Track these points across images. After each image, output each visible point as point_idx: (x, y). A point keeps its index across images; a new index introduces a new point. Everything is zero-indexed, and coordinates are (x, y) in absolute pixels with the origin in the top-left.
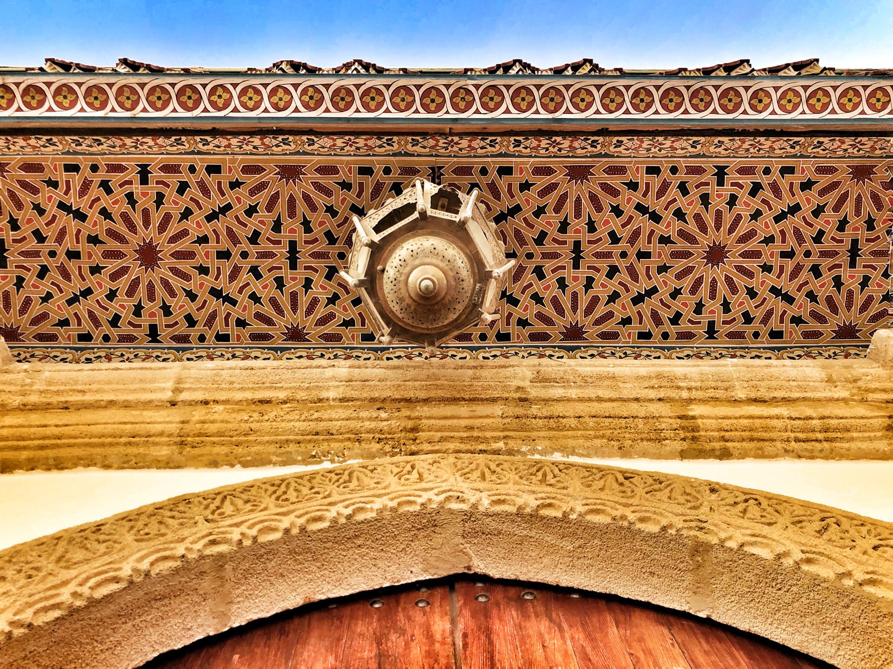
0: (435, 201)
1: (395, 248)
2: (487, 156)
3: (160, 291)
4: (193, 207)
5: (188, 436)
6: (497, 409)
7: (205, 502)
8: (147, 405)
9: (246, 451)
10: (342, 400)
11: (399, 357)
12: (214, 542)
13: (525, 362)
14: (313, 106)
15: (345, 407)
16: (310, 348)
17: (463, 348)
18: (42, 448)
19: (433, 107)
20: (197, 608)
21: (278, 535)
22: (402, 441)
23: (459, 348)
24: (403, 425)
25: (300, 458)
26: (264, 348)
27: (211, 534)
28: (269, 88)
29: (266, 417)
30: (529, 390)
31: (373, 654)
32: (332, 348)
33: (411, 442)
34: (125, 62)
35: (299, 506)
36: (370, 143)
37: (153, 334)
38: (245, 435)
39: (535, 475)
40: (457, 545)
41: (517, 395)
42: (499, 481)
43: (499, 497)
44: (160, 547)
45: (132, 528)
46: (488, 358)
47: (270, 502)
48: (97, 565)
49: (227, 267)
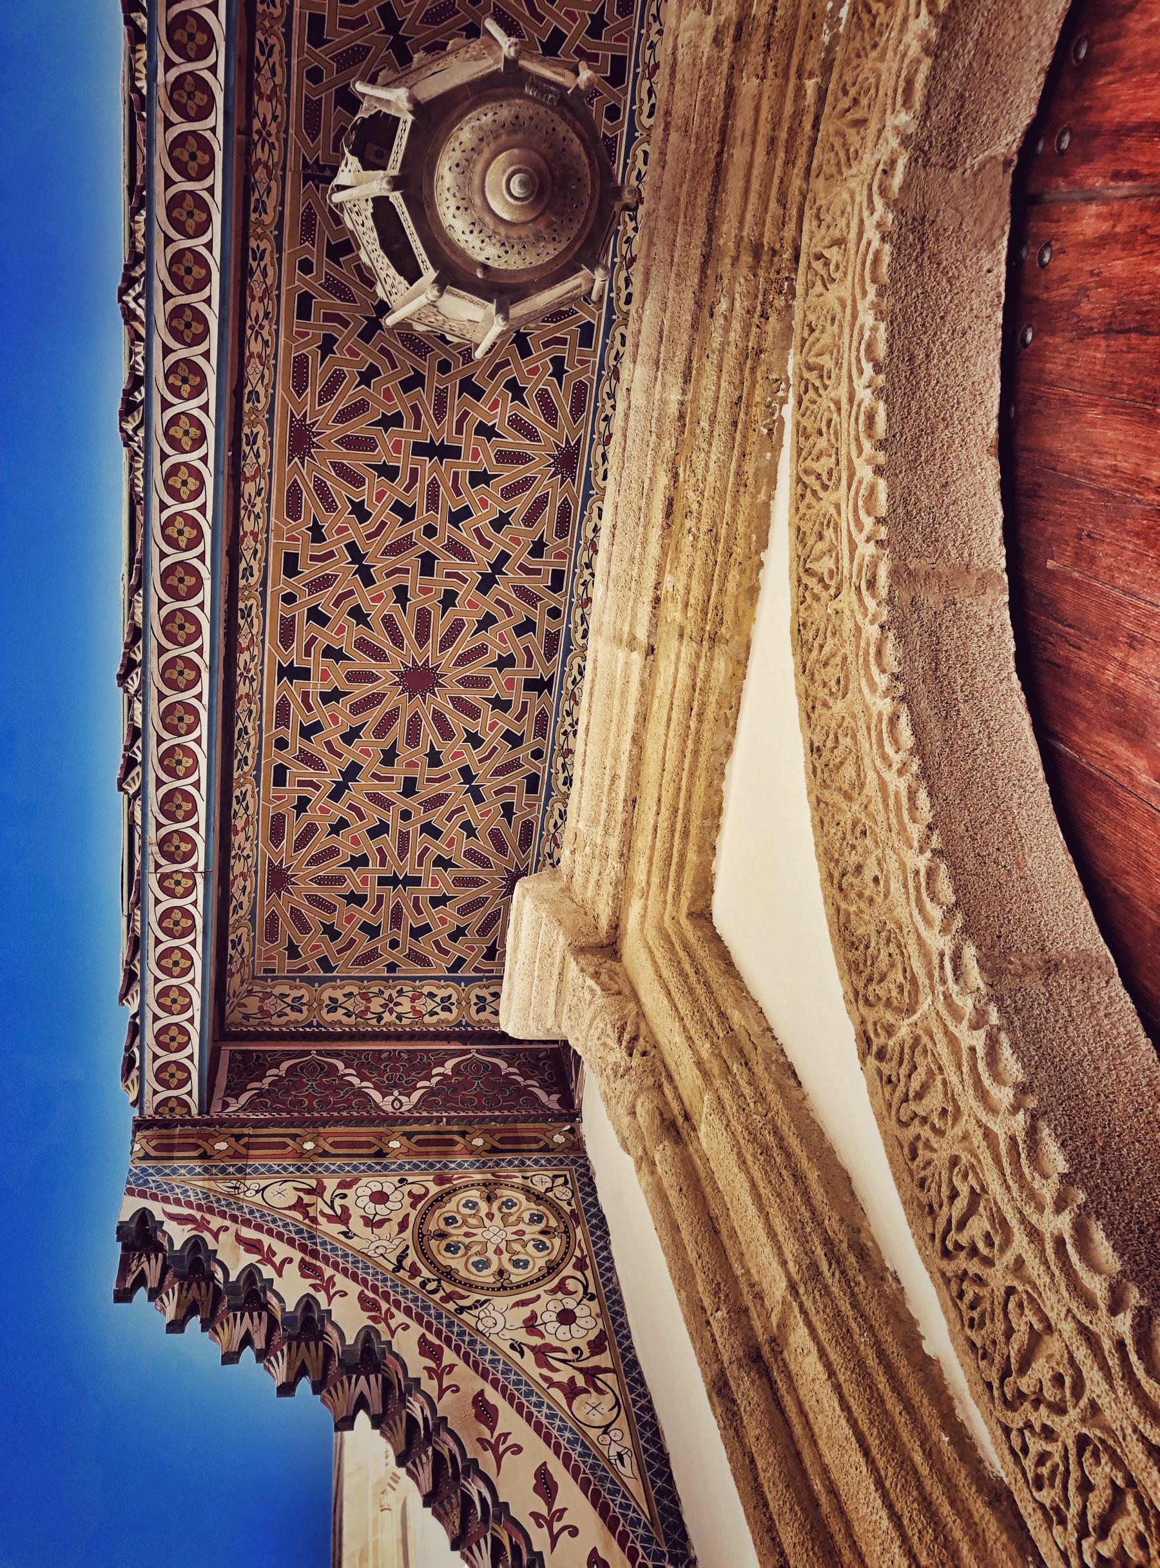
0: (373, 161)
1: (450, 243)
2: (289, 64)
3: (476, 669)
4: (348, 604)
5: (703, 629)
6: (748, 86)
7: (809, 600)
8: (646, 689)
9: (741, 542)
10: (687, 379)
11: (628, 282)
12: (872, 584)
13: (670, 21)
14: (198, 380)
15: (698, 373)
16: (592, 440)
17: (627, 156)
18: (686, 833)
19: (203, 158)
20: (963, 616)
21: (882, 485)
22: (773, 276)
23: (626, 164)
24: (745, 271)
25: (769, 455)
26: (582, 516)
27: (858, 589)
28: (168, 450)
29: (695, 506)
30: (723, 18)
31: (1103, 343)
32: (596, 401)
33: (776, 259)
34: (123, 678)
35: (843, 451)
36: (258, 292)
37: (538, 686)
38: (717, 541)
39: (875, 17)
40: (964, 181)
41: (728, 42)
42: (873, 91)
43: (900, 91)
44: (861, 660)
45: (825, 704)
46: (653, 106)
47: (826, 504)
48: (867, 746)
49: (446, 561)
